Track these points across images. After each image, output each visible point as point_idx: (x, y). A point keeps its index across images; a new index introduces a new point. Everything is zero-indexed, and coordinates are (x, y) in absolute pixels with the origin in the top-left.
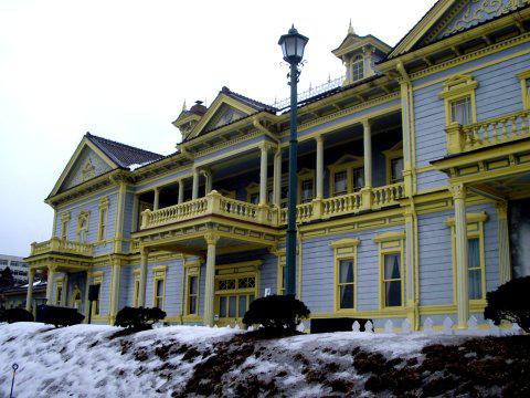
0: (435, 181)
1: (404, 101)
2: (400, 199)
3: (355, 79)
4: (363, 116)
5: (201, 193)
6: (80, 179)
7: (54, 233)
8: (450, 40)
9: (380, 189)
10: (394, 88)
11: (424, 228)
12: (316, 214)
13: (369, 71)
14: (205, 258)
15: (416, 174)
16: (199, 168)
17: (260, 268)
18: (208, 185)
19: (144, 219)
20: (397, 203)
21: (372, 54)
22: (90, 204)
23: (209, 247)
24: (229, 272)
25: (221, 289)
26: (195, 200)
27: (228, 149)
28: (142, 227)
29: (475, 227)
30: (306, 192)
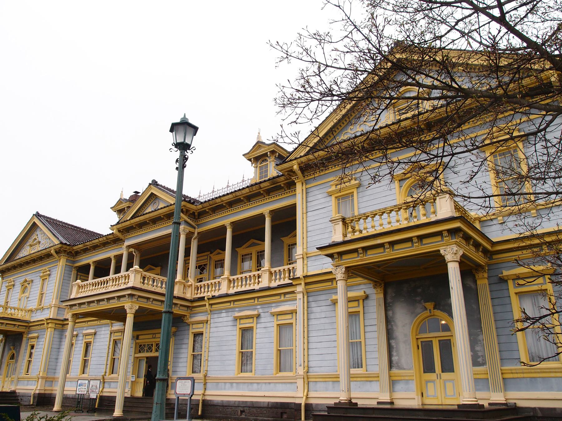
0: (324, 264)
1: (299, 197)
2: (294, 279)
3: (260, 178)
4: (265, 208)
5: (130, 265)
6: (26, 252)
8: (147, 216)
9: (277, 269)
10: (291, 185)
11: (313, 304)
12: (224, 289)
13: (273, 171)
15: (306, 257)
18: (136, 260)
20: (291, 281)
21: (275, 157)
22: (33, 274)
25: (140, 352)
26: (123, 273)
29: (355, 304)
30: (219, 270)
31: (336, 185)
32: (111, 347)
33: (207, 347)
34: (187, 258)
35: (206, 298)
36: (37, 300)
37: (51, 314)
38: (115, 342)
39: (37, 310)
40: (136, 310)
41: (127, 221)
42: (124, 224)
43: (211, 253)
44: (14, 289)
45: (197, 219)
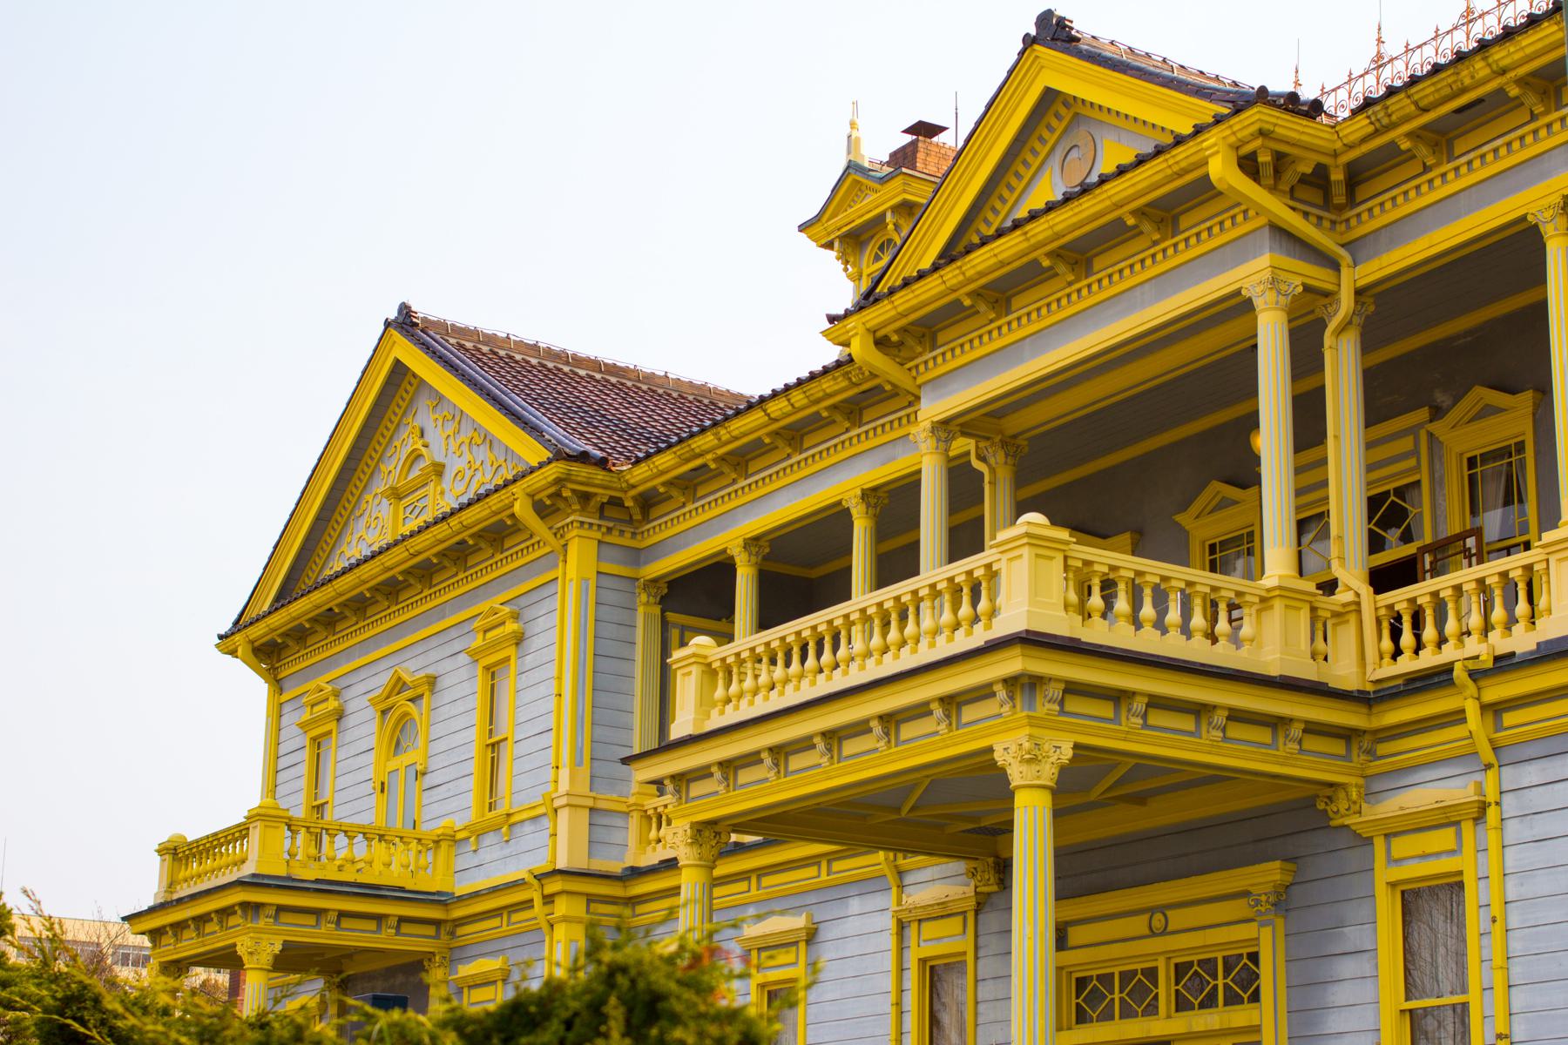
5: (965, 538)
6: (375, 527)
7: (272, 787)
14: (1003, 869)
16: (946, 428)
17: (1282, 901)
18: (996, 499)
19: (686, 688)
22: (432, 647)
23: (1021, 800)
24: (1121, 937)
26: (934, 569)
27: (1165, 283)
28: (677, 731)
31: (485, 632)
32: (911, 1001)
33: (1498, 960)
34: (1311, 455)
35: (1459, 673)
36: (472, 783)
37: (564, 845)
38: (936, 975)
39: (480, 832)
40: (1063, 771)
41: (922, 275)
42: (903, 300)
43: (1437, 413)
44: (349, 736)
45: (1340, 209)
